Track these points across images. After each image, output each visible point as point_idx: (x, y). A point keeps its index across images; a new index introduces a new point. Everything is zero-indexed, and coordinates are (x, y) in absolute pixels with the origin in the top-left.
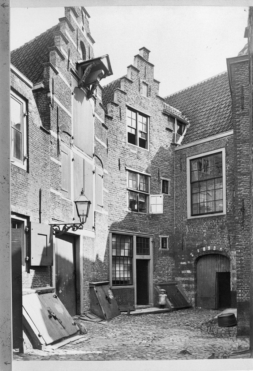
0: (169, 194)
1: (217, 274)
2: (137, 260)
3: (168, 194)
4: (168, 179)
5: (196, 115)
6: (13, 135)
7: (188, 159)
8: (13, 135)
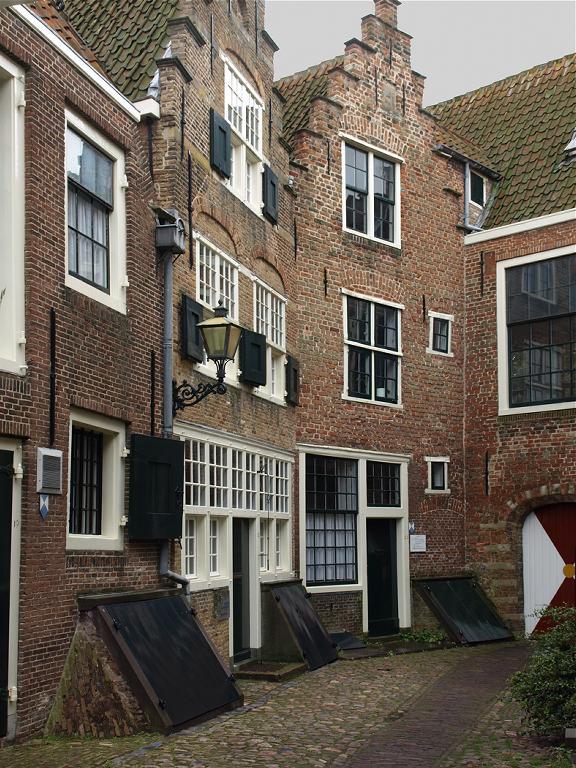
0: (450, 354)
1: (397, 503)
2: (370, 521)
3: (446, 352)
4: (449, 317)
5: (519, 168)
6: (317, 450)
7: (501, 269)
8: (317, 450)
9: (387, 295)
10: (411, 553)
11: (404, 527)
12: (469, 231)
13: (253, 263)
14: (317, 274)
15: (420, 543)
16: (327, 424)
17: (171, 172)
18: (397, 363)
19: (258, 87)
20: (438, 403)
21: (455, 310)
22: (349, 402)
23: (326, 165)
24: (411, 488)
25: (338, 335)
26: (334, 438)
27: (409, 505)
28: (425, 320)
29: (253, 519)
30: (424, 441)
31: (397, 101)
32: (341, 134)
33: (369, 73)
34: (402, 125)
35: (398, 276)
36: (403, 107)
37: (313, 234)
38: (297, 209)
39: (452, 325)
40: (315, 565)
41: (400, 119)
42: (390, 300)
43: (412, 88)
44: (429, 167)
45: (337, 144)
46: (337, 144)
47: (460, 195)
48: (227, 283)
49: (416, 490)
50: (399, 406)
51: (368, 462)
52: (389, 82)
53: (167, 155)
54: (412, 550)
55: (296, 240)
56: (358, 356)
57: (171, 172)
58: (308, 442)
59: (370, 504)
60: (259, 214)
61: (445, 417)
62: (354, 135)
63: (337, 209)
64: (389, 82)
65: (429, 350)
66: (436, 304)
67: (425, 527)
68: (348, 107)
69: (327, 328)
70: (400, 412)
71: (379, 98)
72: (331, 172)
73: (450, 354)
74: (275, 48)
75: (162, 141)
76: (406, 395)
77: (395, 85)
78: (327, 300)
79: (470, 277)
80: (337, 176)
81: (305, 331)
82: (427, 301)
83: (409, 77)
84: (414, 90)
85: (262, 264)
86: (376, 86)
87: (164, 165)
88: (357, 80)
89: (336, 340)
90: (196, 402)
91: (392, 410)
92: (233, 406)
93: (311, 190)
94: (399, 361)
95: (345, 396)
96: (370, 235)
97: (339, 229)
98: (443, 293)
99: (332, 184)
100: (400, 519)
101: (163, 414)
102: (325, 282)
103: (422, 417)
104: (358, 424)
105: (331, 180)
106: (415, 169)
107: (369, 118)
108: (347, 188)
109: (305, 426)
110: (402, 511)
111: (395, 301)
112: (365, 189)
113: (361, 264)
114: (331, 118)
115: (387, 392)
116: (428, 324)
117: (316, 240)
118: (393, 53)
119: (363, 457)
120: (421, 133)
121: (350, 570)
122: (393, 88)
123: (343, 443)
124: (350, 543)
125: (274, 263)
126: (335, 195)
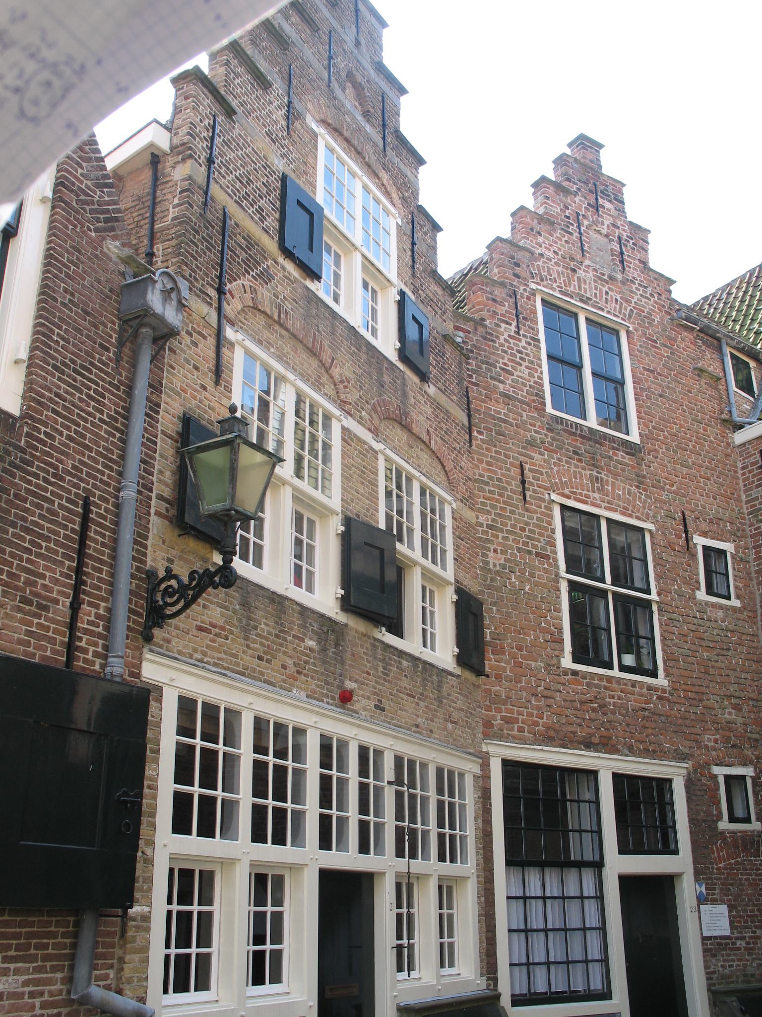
0: (735, 603)
1: (672, 847)
2: (627, 882)
4: (728, 547)
9: (624, 508)
10: (704, 939)
11: (688, 891)
12: (741, 427)
13: (382, 426)
14: (508, 470)
15: (717, 920)
16: (538, 708)
17: (181, 223)
18: (651, 612)
19: (376, 175)
20: (724, 679)
21: (734, 536)
22: (575, 673)
23: (514, 324)
24: (693, 821)
25: (549, 565)
26: (552, 733)
27: (693, 851)
28: (688, 545)
29: (427, 876)
30: (708, 739)
31: (612, 255)
32: (533, 286)
33: (568, 218)
34: (623, 283)
35: (640, 481)
36: (622, 262)
37: (499, 413)
38: (471, 376)
39: (733, 557)
40: (528, 964)
41: (619, 276)
42: (630, 516)
43: (631, 242)
44: (670, 339)
45: (528, 298)
46: (528, 298)
47: (719, 379)
48: (434, 547)
49: (702, 826)
50: (661, 681)
51: (615, 775)
52: (599, 232)
53: (176, 201)
54: (704, 935)
55: (469, 416)
56: (584, 602)
57: (181, 223)
58: (506, 738)
59: (623, 850)
60: (393, 356)
61: (738, 701)
62: (554, 290)
63: (535, 382)
64: (599, 232)
65: (702, 595)
66: (704, 526)
67: (725, 891)
68: (542, 255)
69: (530, 552)
70: (664, 691)
71: (586, 248)
72: (521, 332)
73: (735, 603)
74: (421, 161)
75: (171, 184)
76: (671, 664)
77: (607, 236)
78: (527, 510)
79: (751, 489)
80: (532, 338)
81: (491, 554)
82: (689, 520)
83: (626, 228)
84: (633, 244)
85: (398, 433)
86: (580, 233)
87: (171, 216)
88: (552, 224)
89: (546, 571)
90: (187, 606)
91: (650, 688)
92: (324, 650)
93: (493, 354)
94: (655, 608)
95: (567, 662)
96: (592, 421)
97: (541, 409)
98: (713, 510)
99: (524, 348)
100: (680, 875)
101: (107, 628)
102: (523, 482)
103: (701, 700)
104: (594, 710)
105: (523, 343)
106: (648, 339)
107: (574, 271)
108: (550, 357)
109: (499, 710)
110: (679, 863)
111: (638, 518)
112: (578, 360)
113: (580, 461)
114: (517, 265)
115: (638, 658)
116: (694, 556)
117: (505, 421)
118: (600, 200)
119: (606, 766)
120: (651, 295)
121: (596, 970)
122: (606, 240)
123: (567, 742)
124: (592, 920)
125: (425, 437)
126: (532, 363)
